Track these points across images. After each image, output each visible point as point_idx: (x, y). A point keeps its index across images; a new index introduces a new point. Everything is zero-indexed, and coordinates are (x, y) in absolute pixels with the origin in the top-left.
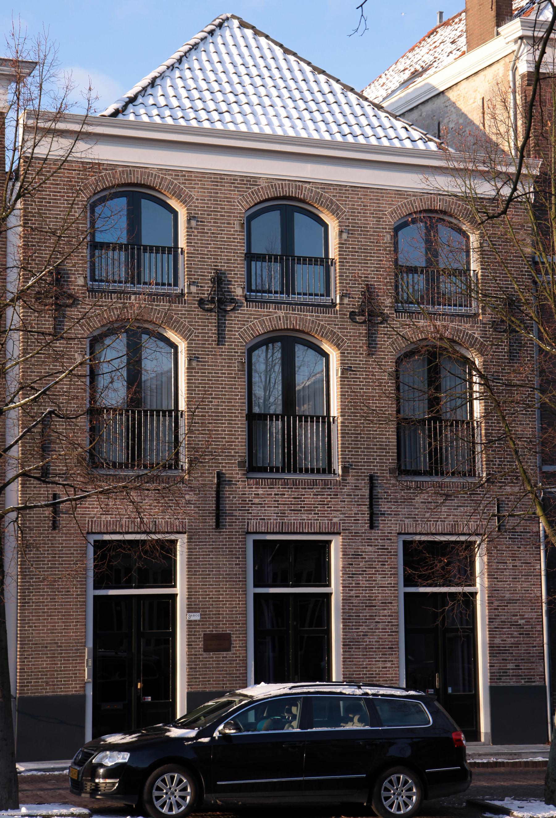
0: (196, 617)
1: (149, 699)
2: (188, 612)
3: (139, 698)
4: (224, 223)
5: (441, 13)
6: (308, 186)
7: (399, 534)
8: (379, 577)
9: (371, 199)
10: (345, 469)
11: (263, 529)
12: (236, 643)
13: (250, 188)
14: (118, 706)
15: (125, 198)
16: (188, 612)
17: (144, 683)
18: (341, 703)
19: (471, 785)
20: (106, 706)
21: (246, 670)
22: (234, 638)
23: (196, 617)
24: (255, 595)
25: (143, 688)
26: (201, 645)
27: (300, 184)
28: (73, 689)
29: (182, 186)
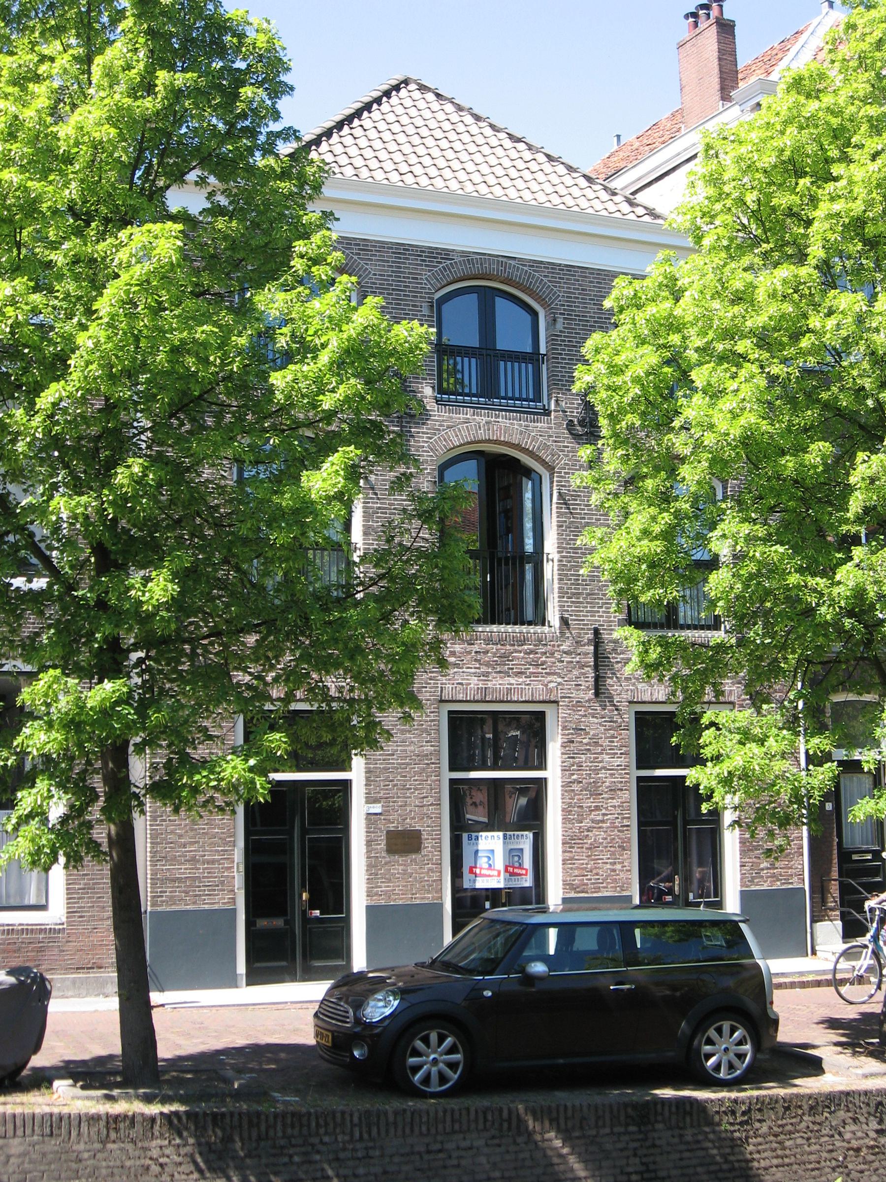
0: (377, 808)
1: (317, 913)
2: (367, 802)
3: (304, 913)
4: (408, 305)
5: (618, 136)
6: (512, 262)
7: (630, 702)
8: (606, 758)
9: (591, 282)
10: (564, 622)
11: (461, 697)
12: (428, 844)
13: (440, 263)
14: (279, 923)
15: (116, 1048)
16: (367, 802)
17: (311, 893)
18: (637, 932)
19: (525, 954)
20: (263, 923)
21: (441, 876)
22: (425, 836)
23: (377, 808)
24: (452, 782)
25: (311, 900)
26: (383, 846)
27: (504, 260)
28: (219, 902)
29: (355, 257)
